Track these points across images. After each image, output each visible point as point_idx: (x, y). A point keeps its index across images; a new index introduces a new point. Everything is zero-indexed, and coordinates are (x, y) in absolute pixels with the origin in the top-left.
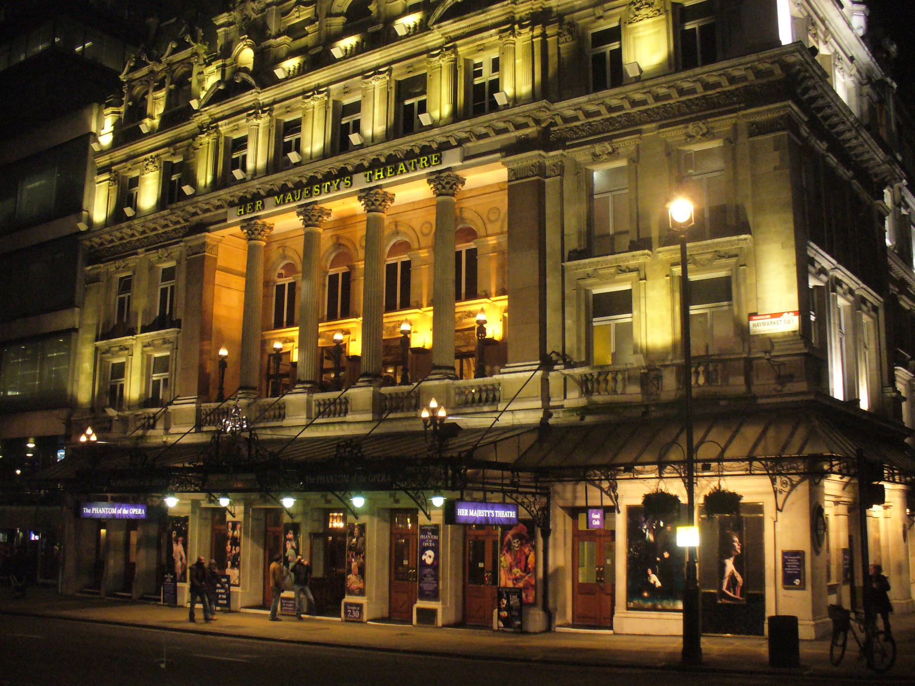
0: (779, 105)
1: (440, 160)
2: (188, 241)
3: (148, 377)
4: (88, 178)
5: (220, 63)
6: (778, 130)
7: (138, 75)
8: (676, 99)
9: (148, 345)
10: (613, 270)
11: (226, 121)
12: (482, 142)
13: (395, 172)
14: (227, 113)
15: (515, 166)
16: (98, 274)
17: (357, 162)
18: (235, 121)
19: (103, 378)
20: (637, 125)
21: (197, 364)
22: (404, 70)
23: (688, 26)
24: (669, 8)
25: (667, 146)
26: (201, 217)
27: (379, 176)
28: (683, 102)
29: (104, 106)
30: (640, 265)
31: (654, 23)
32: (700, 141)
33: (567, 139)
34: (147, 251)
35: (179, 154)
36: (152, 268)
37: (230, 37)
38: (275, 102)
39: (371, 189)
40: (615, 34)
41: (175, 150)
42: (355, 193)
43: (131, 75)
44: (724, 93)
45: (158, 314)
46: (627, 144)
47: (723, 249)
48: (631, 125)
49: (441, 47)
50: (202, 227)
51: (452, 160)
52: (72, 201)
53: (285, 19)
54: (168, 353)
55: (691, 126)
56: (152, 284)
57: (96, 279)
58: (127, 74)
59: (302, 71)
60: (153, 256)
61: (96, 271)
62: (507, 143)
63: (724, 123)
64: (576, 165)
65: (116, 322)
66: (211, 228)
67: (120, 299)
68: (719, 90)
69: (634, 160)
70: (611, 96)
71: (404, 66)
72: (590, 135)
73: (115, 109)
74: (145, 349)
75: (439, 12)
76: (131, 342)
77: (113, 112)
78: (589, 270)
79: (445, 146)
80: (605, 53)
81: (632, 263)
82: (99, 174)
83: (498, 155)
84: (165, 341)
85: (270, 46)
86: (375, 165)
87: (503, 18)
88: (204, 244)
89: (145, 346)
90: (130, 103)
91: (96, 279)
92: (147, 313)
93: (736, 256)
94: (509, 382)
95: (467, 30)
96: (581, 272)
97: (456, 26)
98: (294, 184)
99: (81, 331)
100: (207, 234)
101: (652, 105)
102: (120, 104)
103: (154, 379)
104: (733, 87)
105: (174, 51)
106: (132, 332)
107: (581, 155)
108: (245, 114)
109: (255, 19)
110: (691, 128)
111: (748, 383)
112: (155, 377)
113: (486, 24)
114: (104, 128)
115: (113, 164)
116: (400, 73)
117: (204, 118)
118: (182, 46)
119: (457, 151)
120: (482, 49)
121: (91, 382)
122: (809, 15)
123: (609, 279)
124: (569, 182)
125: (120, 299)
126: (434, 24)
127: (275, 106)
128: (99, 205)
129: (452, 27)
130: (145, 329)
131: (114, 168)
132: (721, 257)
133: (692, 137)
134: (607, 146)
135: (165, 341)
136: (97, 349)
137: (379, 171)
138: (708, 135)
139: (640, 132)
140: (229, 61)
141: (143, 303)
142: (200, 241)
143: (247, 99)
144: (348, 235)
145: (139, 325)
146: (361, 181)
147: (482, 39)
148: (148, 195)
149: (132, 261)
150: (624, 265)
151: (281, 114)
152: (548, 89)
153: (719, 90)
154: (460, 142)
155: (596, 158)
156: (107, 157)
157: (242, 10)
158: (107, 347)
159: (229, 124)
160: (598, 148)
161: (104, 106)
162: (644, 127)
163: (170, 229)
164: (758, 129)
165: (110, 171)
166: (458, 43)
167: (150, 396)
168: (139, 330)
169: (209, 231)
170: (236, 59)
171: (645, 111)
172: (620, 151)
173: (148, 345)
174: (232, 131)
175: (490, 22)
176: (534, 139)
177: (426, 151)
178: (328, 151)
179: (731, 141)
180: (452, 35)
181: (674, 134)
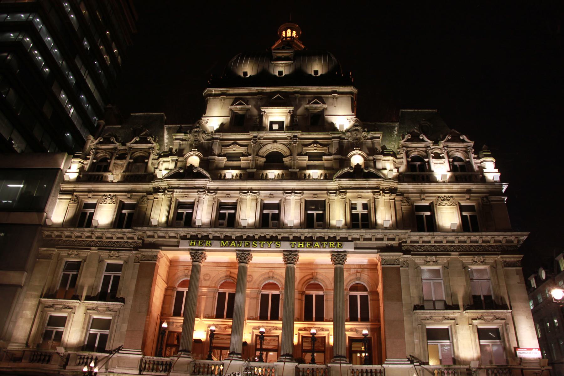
0: (517, 256)
1: (341, 246)
2: (141, 251)
3: (87, 330)
4: (52, 194)
5: (175, 158)
6: (517, 266)
7: (104, 147)
8: (468, 243)
9: (93, 309)
10: (441, 318)
11: (181, 190)
12: (365, 242)
13: (311, 245)
14: (181, 186)
15: (386, 258)
16: (51, 254)
17: (286, 235)
18: (188, 192)
19: (42, 323)
20: (448, 251)
21: (143, 329)
22: (312, 196)
23: (464, 214)
24: (118, 202)
25: (463, 264)
26: (155, 239)
27: (301, 246)
28: (472, 246)
29: (72, 156)
30: (456, 317)
31: (450, 208)
32: (479, 265)
33: (411, 251)
34: (99, 249)
35: (133, 199)
36: (101, 261)
37: (182, 147)
38: (218, 189)
39: (292, 251)
40: (94, 206)
41: (131, 196)
42: (280, 252)
43: (99, 146)
44: (491, 246)
45: (100, 291)
46: (443, 259)
47: (498, 315)
48: (446, 251)
49: (336, 190)
50: (156, 246)
51: (348, 247)
52: (37, 204)
53: (224, 148)
54: (110, 318)
55: (476, 257)
56: (99, 271)
57: (48, 257)
58: (96, 144)
59: (282, 178)
60: (104, 254)
61: (50, 252)
62: (380, 246)
63: (491, 259)
64: (415, 264)
65: (58, 288)
66: (163, 248)
67: (64, 274)
68: (488, 244)
69: (446, 267)
70: (426, 236)
71: (311, 194)
72: (424, 251)
73: (81, 161)
74: (88, 311)
75: (340, 173)
76: (74, 305)
77: (80, 162)
78: (428, 316)
79: (345, 240)
80: (87, 213)
81: (452, 316)
82: (60, 194)
83: (376, 251)
84: (109, 310)
85: (214, 159)
86: (297, 239)
87: (375, 186)
88: (156, 256)
89: (88, 309)
90: (95, 161)
91: (48, 257)
92: (92, 288)
93: (72, 308)
94: (392, 369)
95: (353, 186)
96: (423, 316)
97: (348, 182)
98: (236, 237)
99: (25, 288)
100: (160, 251)
101: (456, 244)
102: (86, 159)
103: (91, 332)
104: (494, 244)
105: (136, 142)
106: (77, 297)
107: (418, 259)
108: (197, 190)
109: (202, 143)
110: (476, 258)
112: (92, 331)
113: (365, 186)
114: (72, 169)
115: (75, 191)
116: (308, 196)
117: (164, 184)
118: (144, 140)
119: (352, 243)
120: (360, 197)
121: (31, 325)
123: (60, 310)
124: (411, 271)
125: (64, 274)
126: (337, 178)
127: (218, 192)
128: (59, 212)
129: (345, 182)
130: (88, 298)
131: (75, 193)
132: (498, 319)
133: (476, 262)
134: (434, 258)
135: (109, 310)
136: (40, 302)
137: (301, 243)
138: (483, 263)
139: (450, 255)
140: (181, 159)
141: (89, 280)
142: (154, 254)
144: (304, 271)
145: (84, 295)
146: (286, 246)
147: (363, 192)
148: (104, 215)
149: (84, 253)
150: (447, 316)
151: (221, 197)
152: (467, 225)
153: (488, 244)
154: (353, 240)
155: (427, 263)
156: (72, 186)
157: (196, 136)
158: (51, 304)
159: (182, 192)
160: (428, 258)
161: (72, 156)
162: (452, 253)
163: (113, 241)
164: (508, 265)
165: (73, 195)
167: (86, 343)
168: (84, 298)
169: (162, 250)
170: (186, 159)
171: (452, 246)
172: (439, 262)
173: (93, 309)
174: (182, 197)
175: (367, 186)
176: (395, 247)
177: (333, 239)
178: (257, 224)
179: (494, 267)
180: (344, 186)
181: (466, 259)
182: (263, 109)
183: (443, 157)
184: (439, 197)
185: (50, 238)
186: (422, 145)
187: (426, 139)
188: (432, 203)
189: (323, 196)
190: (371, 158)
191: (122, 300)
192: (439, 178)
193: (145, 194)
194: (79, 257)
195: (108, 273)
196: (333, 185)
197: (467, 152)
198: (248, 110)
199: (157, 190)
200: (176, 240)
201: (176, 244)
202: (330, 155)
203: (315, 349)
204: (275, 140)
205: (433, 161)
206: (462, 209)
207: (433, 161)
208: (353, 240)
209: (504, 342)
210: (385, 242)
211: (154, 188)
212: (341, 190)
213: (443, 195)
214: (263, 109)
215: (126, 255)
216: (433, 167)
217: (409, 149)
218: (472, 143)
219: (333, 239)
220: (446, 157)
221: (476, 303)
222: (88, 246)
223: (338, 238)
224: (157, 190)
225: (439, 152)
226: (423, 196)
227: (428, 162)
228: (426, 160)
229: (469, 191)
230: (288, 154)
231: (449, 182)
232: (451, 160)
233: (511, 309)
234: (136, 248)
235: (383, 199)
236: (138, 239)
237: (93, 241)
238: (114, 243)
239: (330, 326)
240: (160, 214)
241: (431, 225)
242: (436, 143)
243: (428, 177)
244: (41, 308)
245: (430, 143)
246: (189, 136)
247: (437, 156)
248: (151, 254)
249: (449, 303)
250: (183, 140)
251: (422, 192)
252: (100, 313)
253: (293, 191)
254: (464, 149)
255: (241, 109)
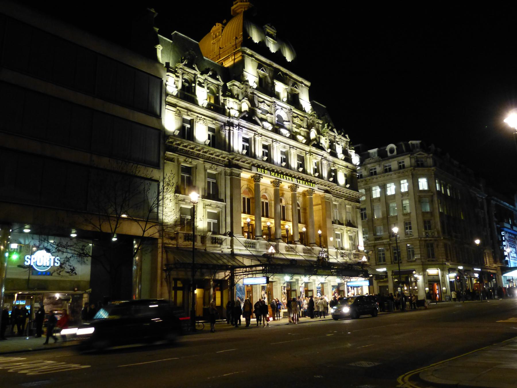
8: (348, 195)
14: (246, 126)
50: (240, 167)
51: (315, 187)
60: (208, 165)
63: (353, 204)
69: (340, 204)
79: (314, 183)
129: (314, 149)
134: (190, 160)
142: (239, 173)
146: (295, 181)
149: (195, 162)
155: (185, 161)
158: (182, 198)
166: (244, 129)
179: (353, 208)
181: (347, 202)
182: (275, 81)
183: (203, 87)
184: (198, 116)
185: (170, 144)
186: (193, 72)
187: (220, 79)
188: (193, 120)
189: (303, 155)
190: (318, 136)
191: (221, 201)
192: (200, 103)
193: (223, 124)
194: (191, 164)
195: (209, 180)
196: (307, 148)
197: (218, 89)
198: (266, 77)
199: (231, 124)
200: (248, 165)
201: (248, 168)
202: (303, 128)
203: (116, 220)
204: (282, 108)
205: (198, 88)
206: (210, 129)
207: (198, 88)
208: (318, 184)
209: (355, 242)
210: (327, 188)
211: (228, 122)
212: (311, 153)
213: (340, 166)
214: (275, 81)
215: (220, 169)
216: (197, 93)
217: (185, 72)
218: (349, 140)
219: (311, 182)
220: (206, 88)
221: (350, 224)
222: (198, 156)
223: (271, 169)
224: (231, 124)
225: (202, 81)
226: (189, 113)
227: (195, 87)
228: (193, 85)
229: (347, 167)
230: (287, 120)
231: (206, 108)
232: (184, 81)
233: (225, 202)
234: (226, 166)
235: (325, 162)
236: (228, 159)
237: (200, 154)
238: (213, 158)
239: (273, 221)
240: (237, 145)
241: (335, 181)
242: (202, 74)
243: (193, 101)
244: (178, 202)
245: (336, 134)
246: (242, 86)
247: (200, 84)
248: (237, 172)
249: (341, 222)
250: (239, 87)
251: (334, 163)
252: (213, 208)
253: (293, 147)
254: (216, 86)
255: (263, 75)
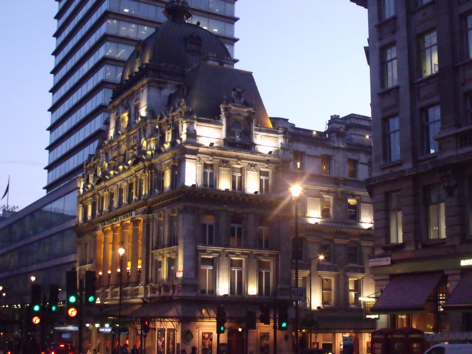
107: (129, 244)
111: (174, 292)
122: (249, 164)
143: (103, 184)
